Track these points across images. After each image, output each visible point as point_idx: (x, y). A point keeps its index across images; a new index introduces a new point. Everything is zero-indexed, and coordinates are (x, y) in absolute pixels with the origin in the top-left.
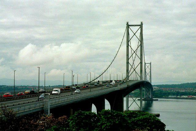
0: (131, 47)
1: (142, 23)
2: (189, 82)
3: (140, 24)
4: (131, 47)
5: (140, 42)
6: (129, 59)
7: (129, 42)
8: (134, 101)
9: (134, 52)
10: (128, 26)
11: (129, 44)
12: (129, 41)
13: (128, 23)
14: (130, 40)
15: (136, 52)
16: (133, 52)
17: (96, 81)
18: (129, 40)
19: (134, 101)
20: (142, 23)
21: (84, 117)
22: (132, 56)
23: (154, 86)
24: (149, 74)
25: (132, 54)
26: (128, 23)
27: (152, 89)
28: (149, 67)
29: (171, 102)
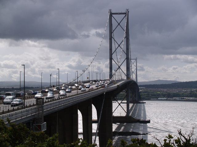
2: (141, 85)
3: (135, 58)
6: (112, 54)
7: (113, 34)
10: (111, 14)
11: (113, 36)
12: (112, 33)
14: (113, 31)
16: (117, 46)
18: (112, 31)
19: (120, 104)
20: (127, 10)
23: (141, 86)
26: (110, 10)
27: (139, 90)
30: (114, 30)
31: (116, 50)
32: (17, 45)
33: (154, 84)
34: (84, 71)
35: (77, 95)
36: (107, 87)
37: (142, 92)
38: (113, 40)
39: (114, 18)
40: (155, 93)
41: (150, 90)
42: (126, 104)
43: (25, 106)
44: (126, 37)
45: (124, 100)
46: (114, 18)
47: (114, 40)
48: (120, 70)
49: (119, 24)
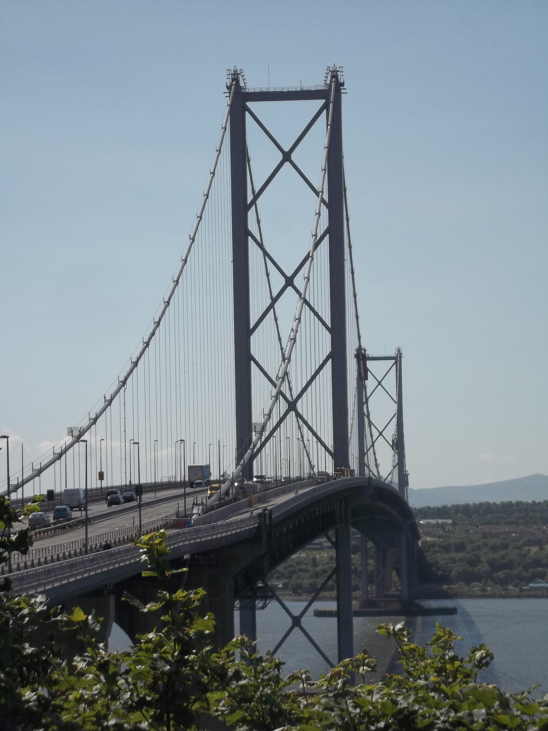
0: (261, 245)
1: (335, 75)
2: (432, 505)
3: (393, 353)
4: (261, 245)
5: (325, 212)
7: (251, 214)
8: (296, 621)
9: (289, 282)
11: (252, 226)
13: (235, 77)
14: (256, 197)
15: (299, 281)
16: (278, 282)
17: (29, 491)
18: (250, 197)
19: (296, 621)
20: (335, 75)
21: (84, 654)
22: (275, 294)
23: (427, 512)
24: (239, 513)
25: (274, 300)
26: (235, 77)
28: (390, 383)
29: (106, 521)
30: (257, 189)
31: (271, 306)
32: (444, 504)
33: (506, 500)
34: (76, 433)
35: (81, 553)
36: (197, 522)
37: (433, 545)
38: (253, 249)
39: (320, 319)
40: (513, 554)
41: (485, 536)
42: (334, 621)
43: (89, 547)
44: (398, 464)
45: (321, 599)
46: (320, 319)
47: (266, 254)
48: (288, 396)
49: (287, 157)
